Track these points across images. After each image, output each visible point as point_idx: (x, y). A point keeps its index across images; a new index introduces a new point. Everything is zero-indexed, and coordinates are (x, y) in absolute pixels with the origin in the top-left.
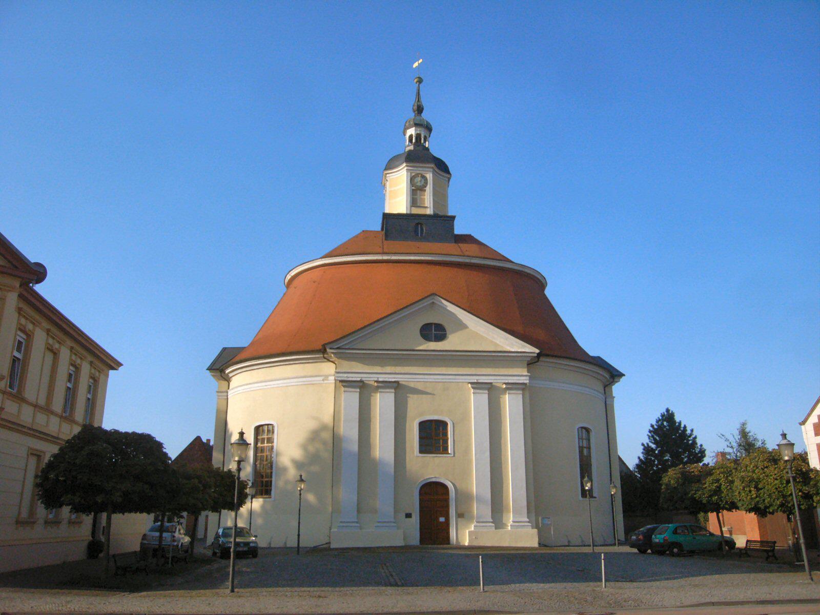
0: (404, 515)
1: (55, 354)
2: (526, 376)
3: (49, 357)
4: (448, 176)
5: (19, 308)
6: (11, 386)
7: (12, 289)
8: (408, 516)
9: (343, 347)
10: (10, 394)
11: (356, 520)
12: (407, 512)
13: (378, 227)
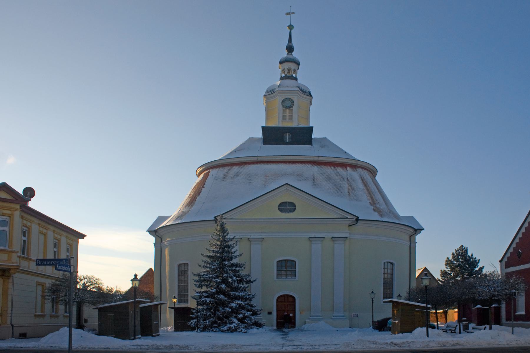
0: (267, 313)
1: (45, 235)
2: (347, 233)
3: (42, 237)
4: (310, 98)
5: (21, 216)
6: (24, 253)
7: (17, 209)
8: (270, 313)
9: (226, 218)
10: (23, 257)
11: (343, 315)
12: (269, 311)
13: (260, 135)
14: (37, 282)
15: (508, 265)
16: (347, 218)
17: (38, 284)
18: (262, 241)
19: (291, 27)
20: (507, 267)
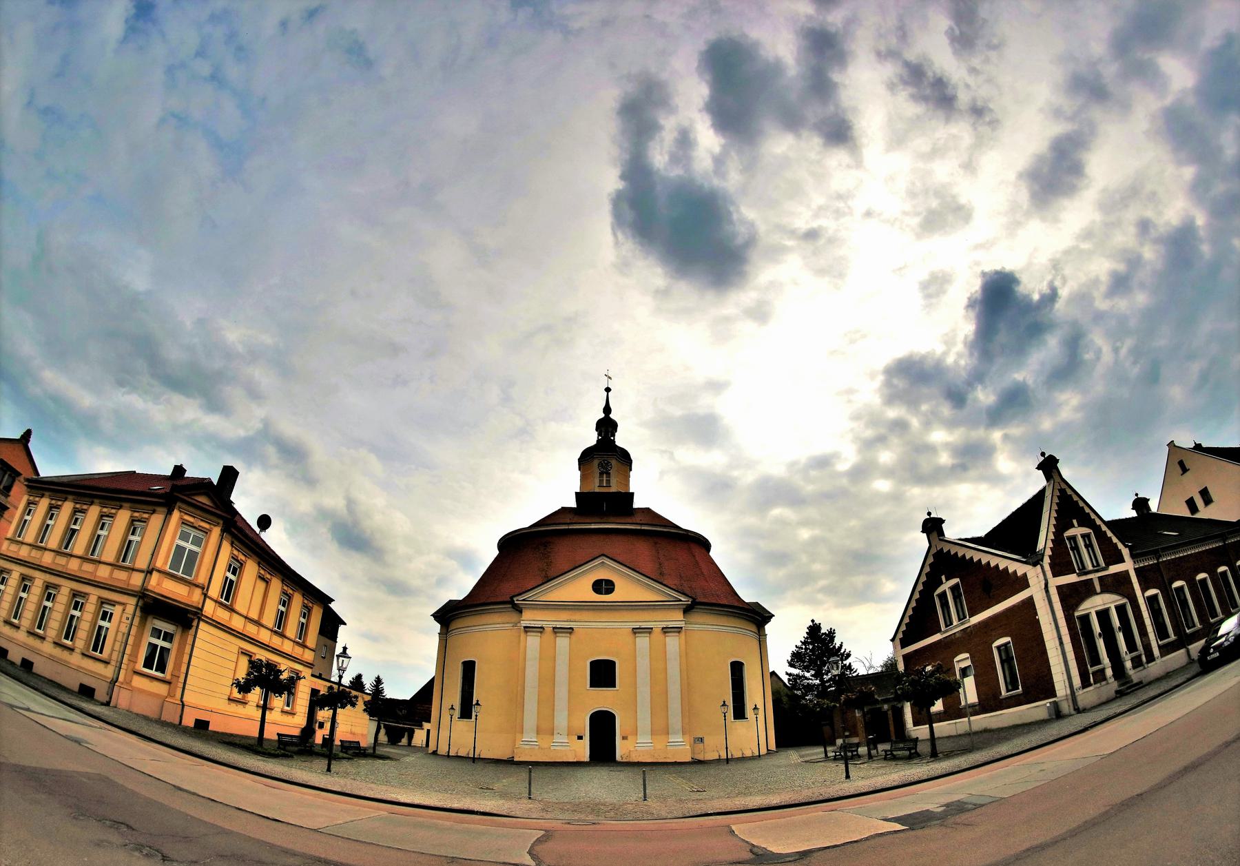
8: (580, 738)
13: (573, 504)
14: (240, 648)
15: (904, 643)
16: (681, 601)
17: (244, 653)
18: (570, 633)
19: (608, 390)
20: (903, 647)
